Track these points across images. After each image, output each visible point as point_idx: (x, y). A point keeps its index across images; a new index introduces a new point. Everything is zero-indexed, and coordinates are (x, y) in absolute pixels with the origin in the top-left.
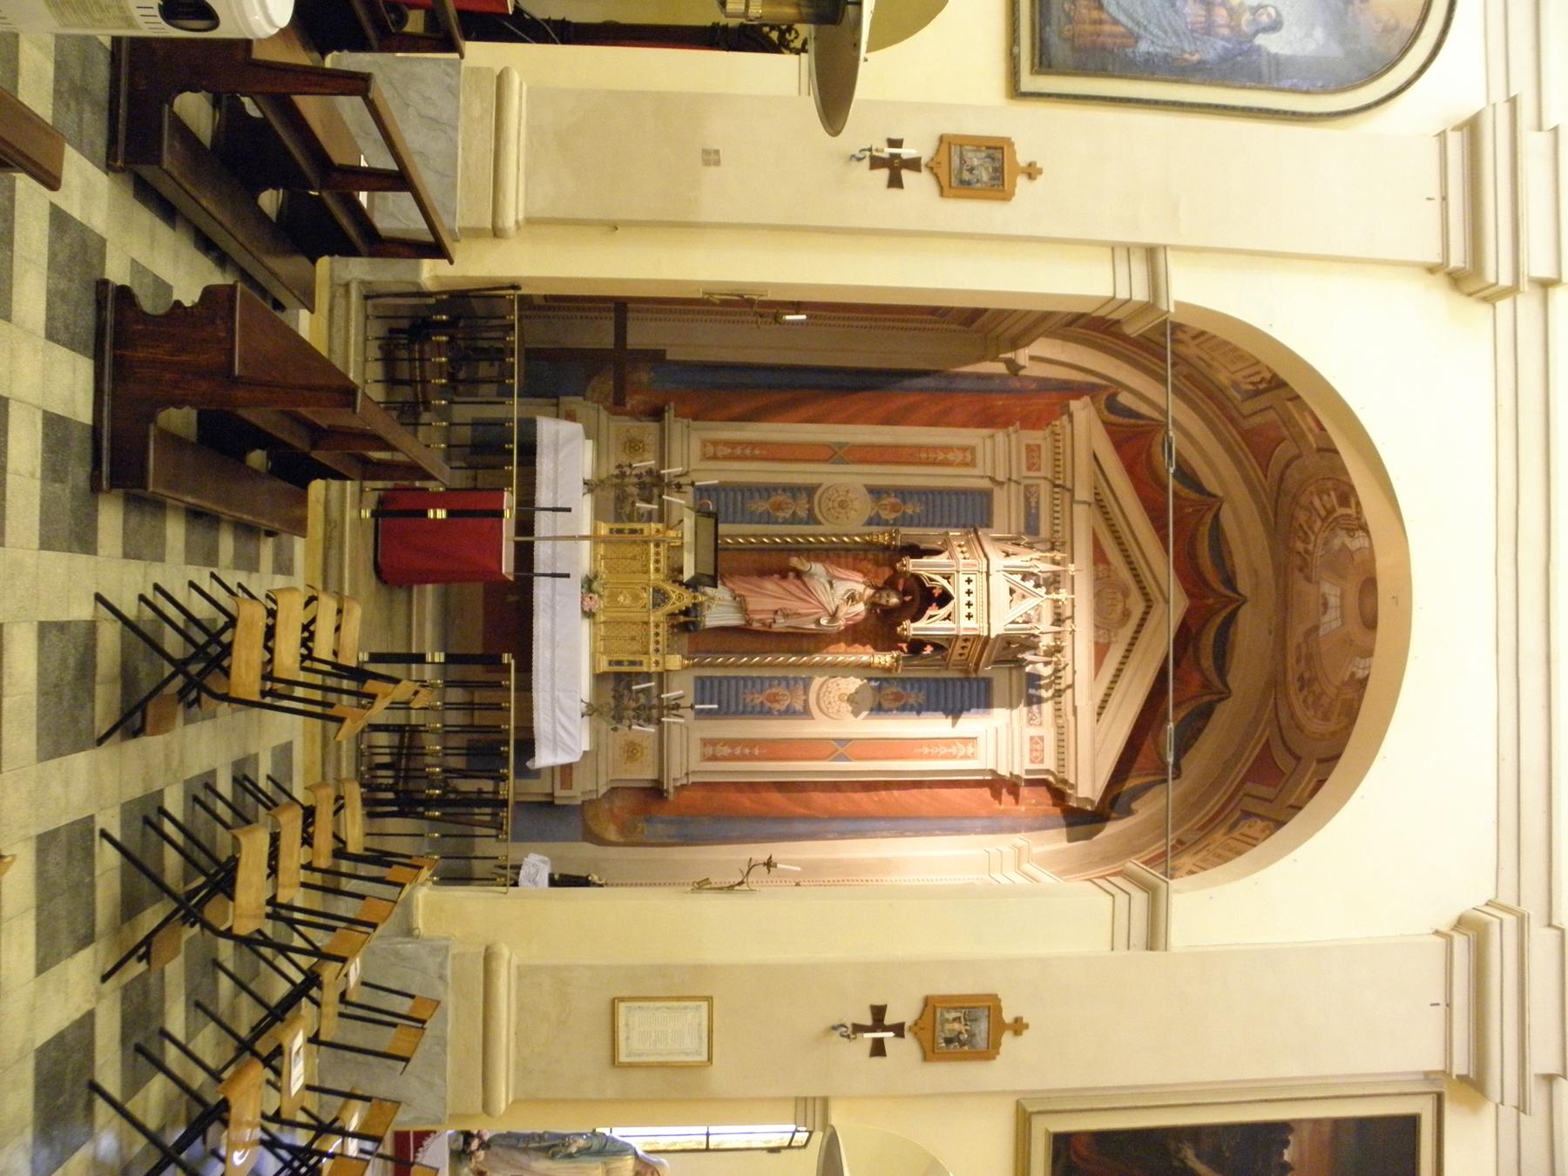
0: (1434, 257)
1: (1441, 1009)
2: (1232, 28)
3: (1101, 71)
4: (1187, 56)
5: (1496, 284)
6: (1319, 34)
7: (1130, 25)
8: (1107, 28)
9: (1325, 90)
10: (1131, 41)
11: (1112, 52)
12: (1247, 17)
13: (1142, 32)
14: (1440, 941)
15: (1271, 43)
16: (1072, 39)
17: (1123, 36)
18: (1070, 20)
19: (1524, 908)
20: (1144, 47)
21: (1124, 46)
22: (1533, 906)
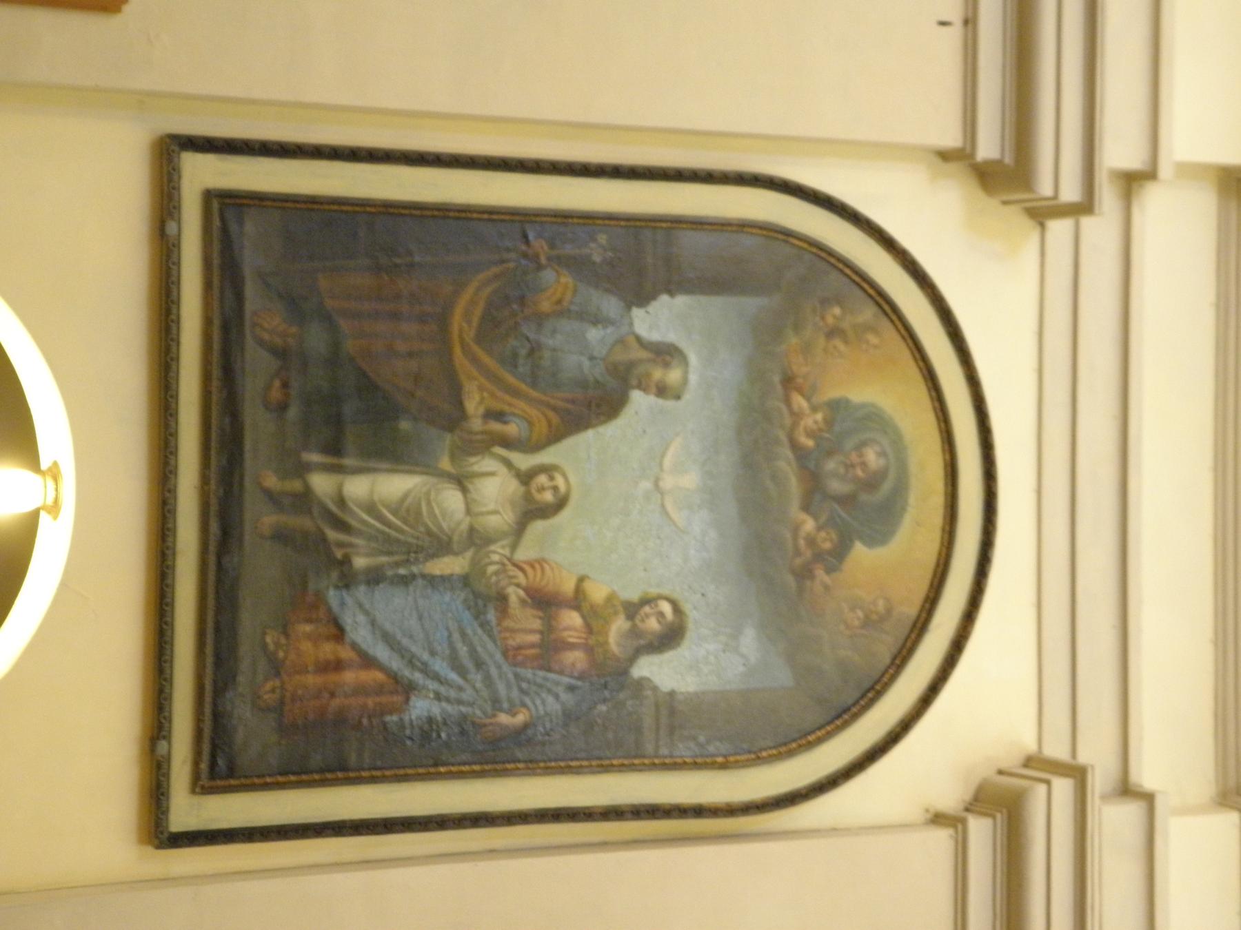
0: (951, 138)
1: (956, 32)
2: (589, 650)
3: (338, 772)
4: (504, 718)
5: (1056, 197)
6: (749, 640)
7: (396, 664)
8: (349, 677)
9: (758, 758)
10: (398, 699)
11: (358, 726)
12: (619, 625)
13: (418, 677)
14: (942, 838)
15: (663, 672)
16: (279, 708)
17: (379, 690)
18: (276, 668)
19: (1083, 758)
20: (421, 707)
21: (383, 711)
22: (1097, 754)
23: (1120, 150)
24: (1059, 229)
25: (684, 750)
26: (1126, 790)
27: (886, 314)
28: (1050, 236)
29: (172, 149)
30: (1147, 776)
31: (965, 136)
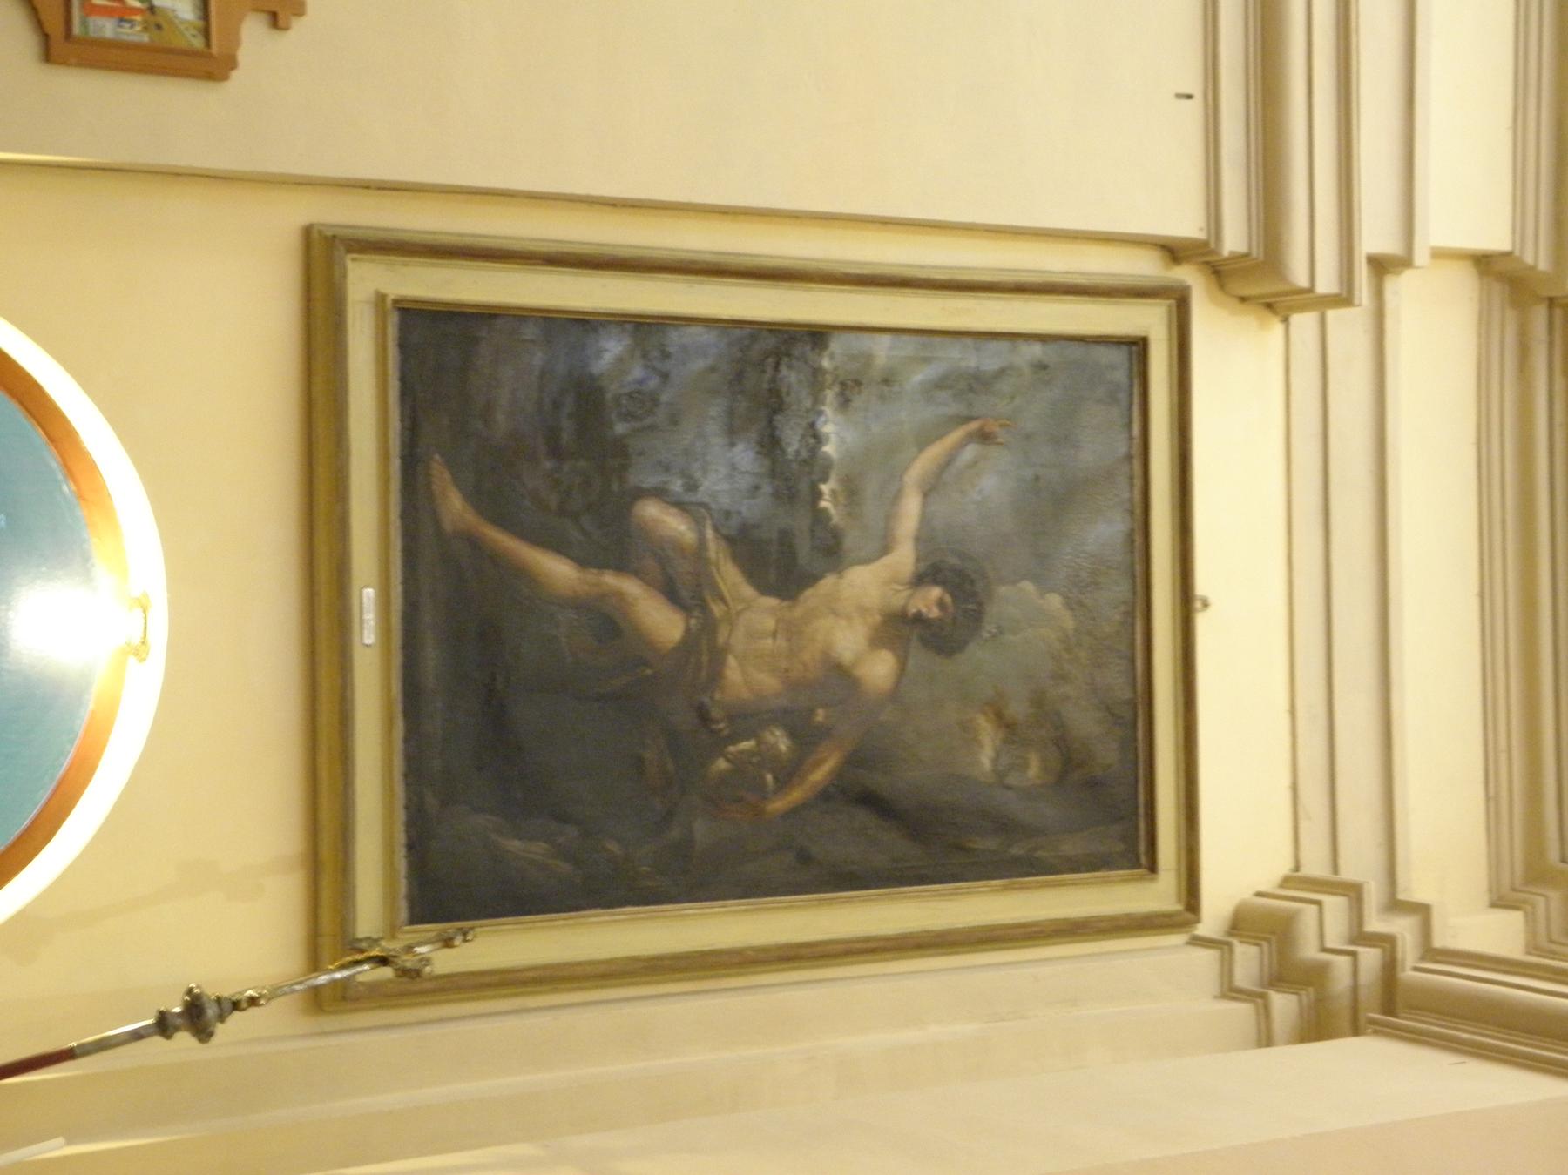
5: (1311, 290)
19: (1348, 874)
23: (1376, 236)
24: (1304, 322)
25: (1036, 350)
26: (1395, 905)
27: (1133, 576)
28: (1293, 329)
29: (323, 259)
30: (1416, 888)
31: (1341, 283)
